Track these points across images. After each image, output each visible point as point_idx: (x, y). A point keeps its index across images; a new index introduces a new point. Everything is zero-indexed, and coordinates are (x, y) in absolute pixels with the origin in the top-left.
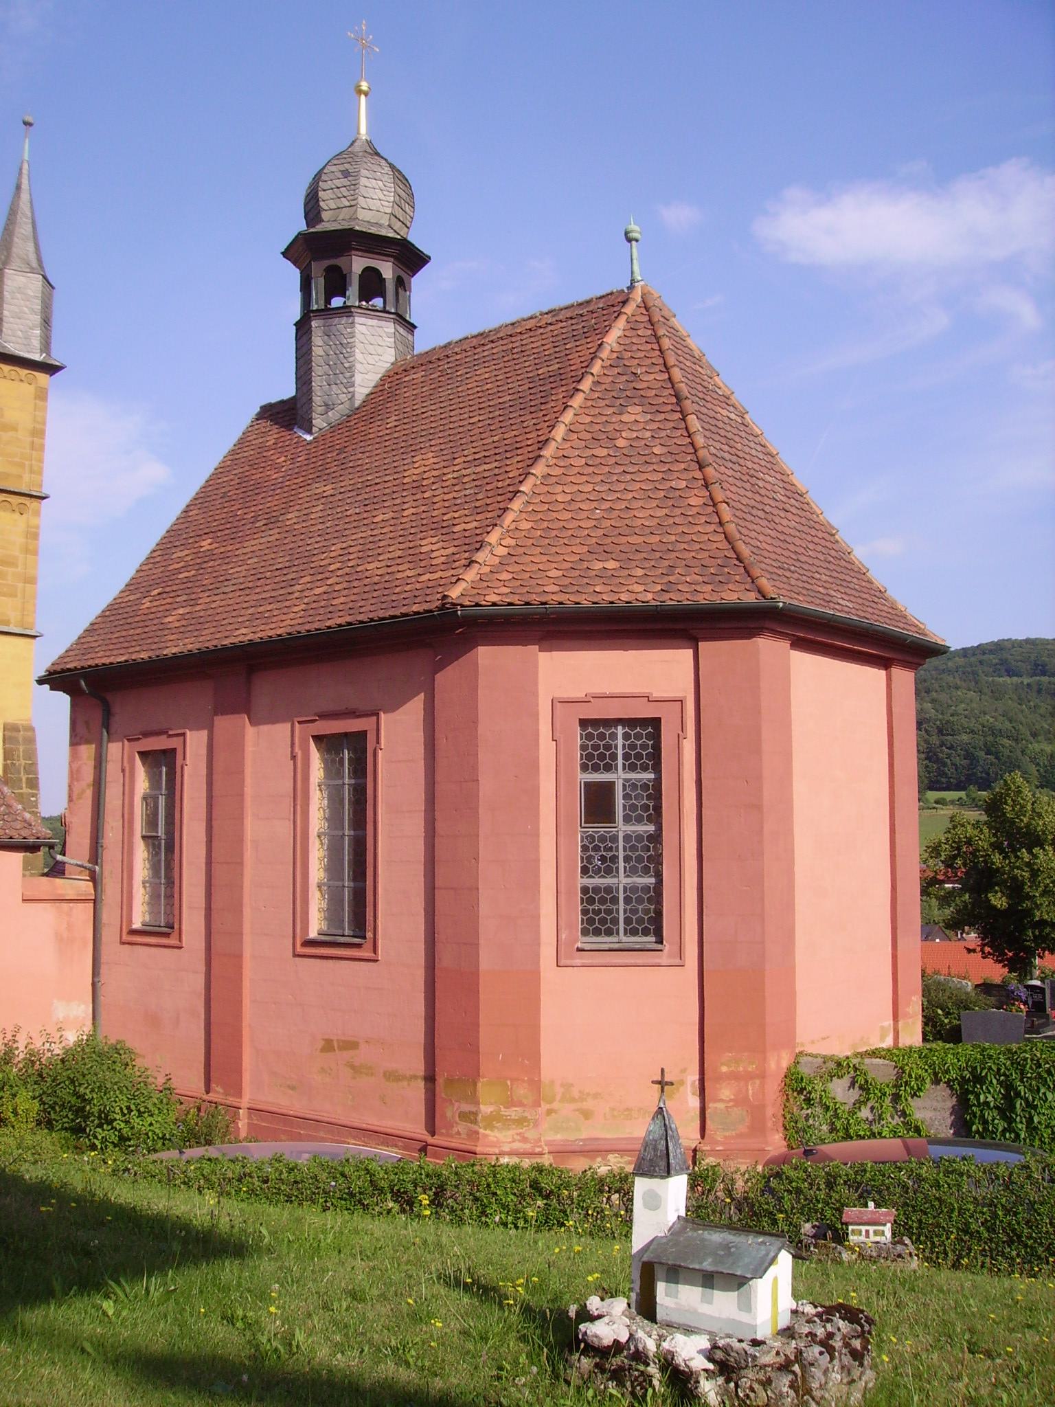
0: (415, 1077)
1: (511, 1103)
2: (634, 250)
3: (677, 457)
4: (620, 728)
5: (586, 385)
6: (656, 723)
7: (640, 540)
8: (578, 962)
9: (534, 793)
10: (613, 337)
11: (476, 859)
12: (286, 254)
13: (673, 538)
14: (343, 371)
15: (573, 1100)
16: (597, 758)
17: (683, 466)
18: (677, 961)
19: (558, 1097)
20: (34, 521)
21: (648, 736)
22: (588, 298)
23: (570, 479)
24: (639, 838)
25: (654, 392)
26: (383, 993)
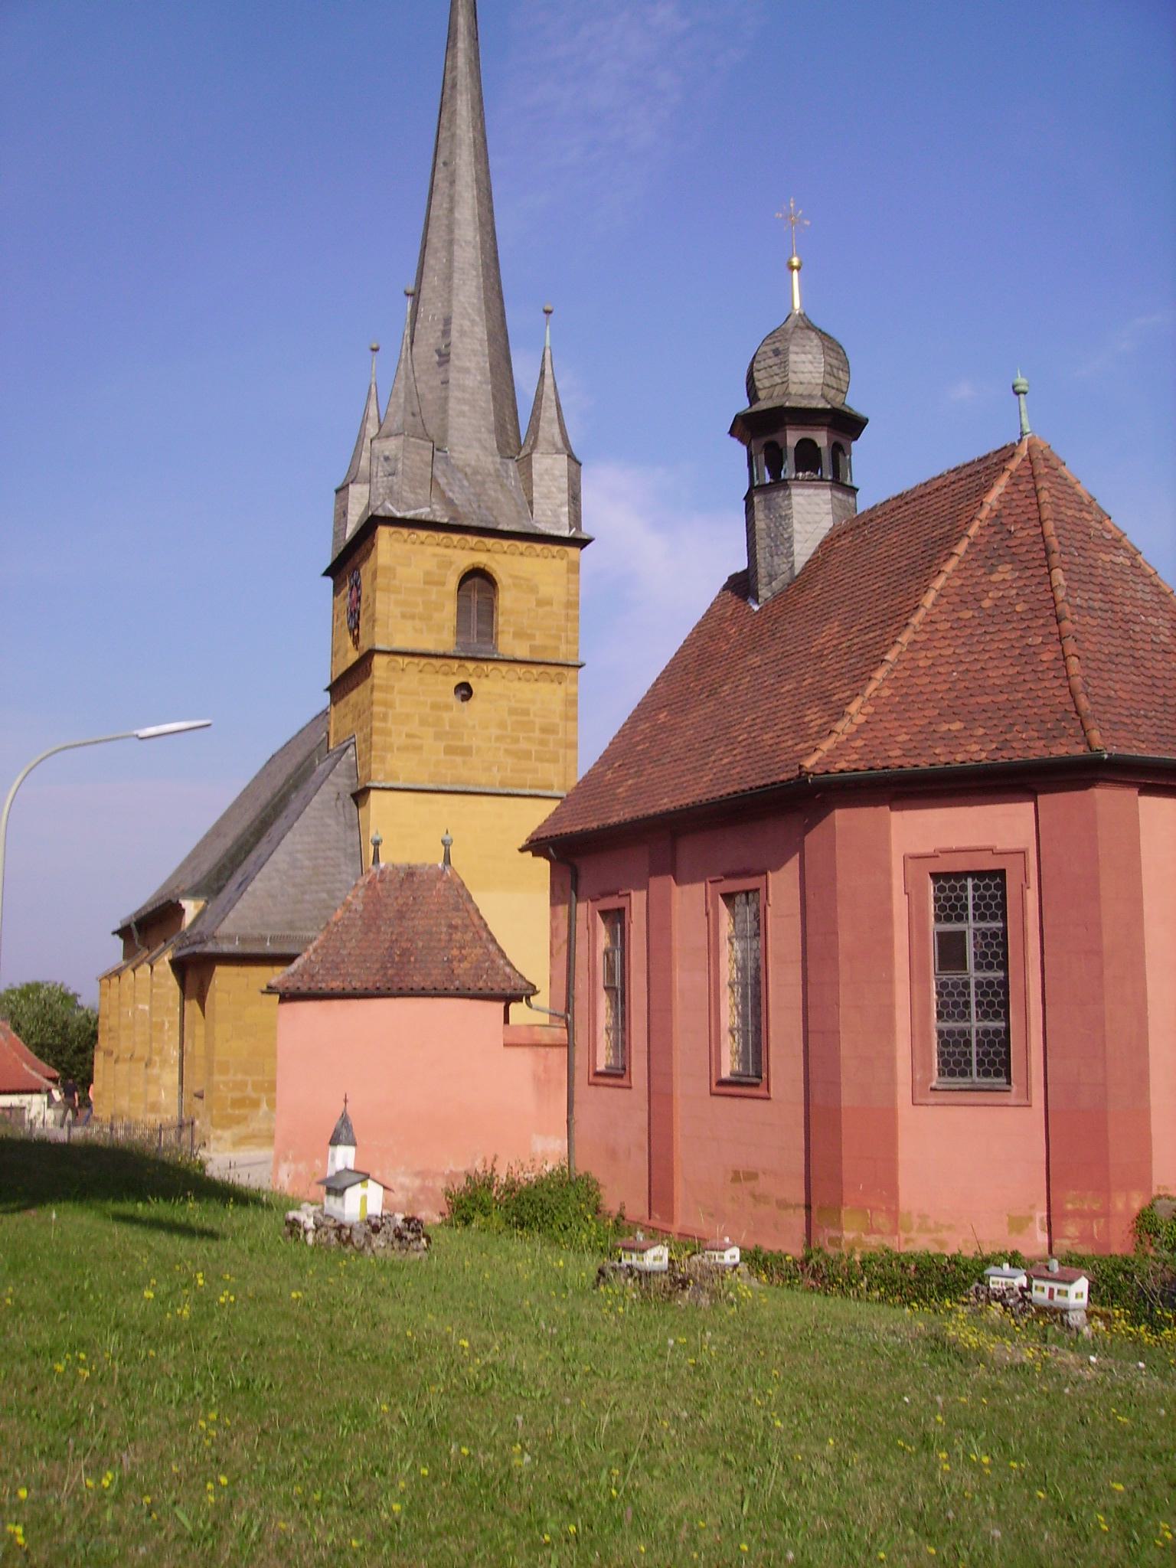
0: (798, 1206)
1: (871, 1230)
2: (1023, 404)
3: (1037, 613)
4: (970, 880)
5: (961, 548)
6: (1001, 873)
7: (986, 699)
8: (932, 1100)
9: (888, 942)
10: (992, 498)
11: (838, 1005)
12: (732, 433)
13: (1020, 695)
14: (783, 541)
15: (929, 1230)
16: (949, 909)
17: (1041, 621)
18: (1024, 1102)
19: (915, 1227)
20: (573, 689)
21: (997, 887)
22: (985, 453)
23: (935, 644)
24: (990, 984)
25: (1025, 549)
26: (771, 1130)
